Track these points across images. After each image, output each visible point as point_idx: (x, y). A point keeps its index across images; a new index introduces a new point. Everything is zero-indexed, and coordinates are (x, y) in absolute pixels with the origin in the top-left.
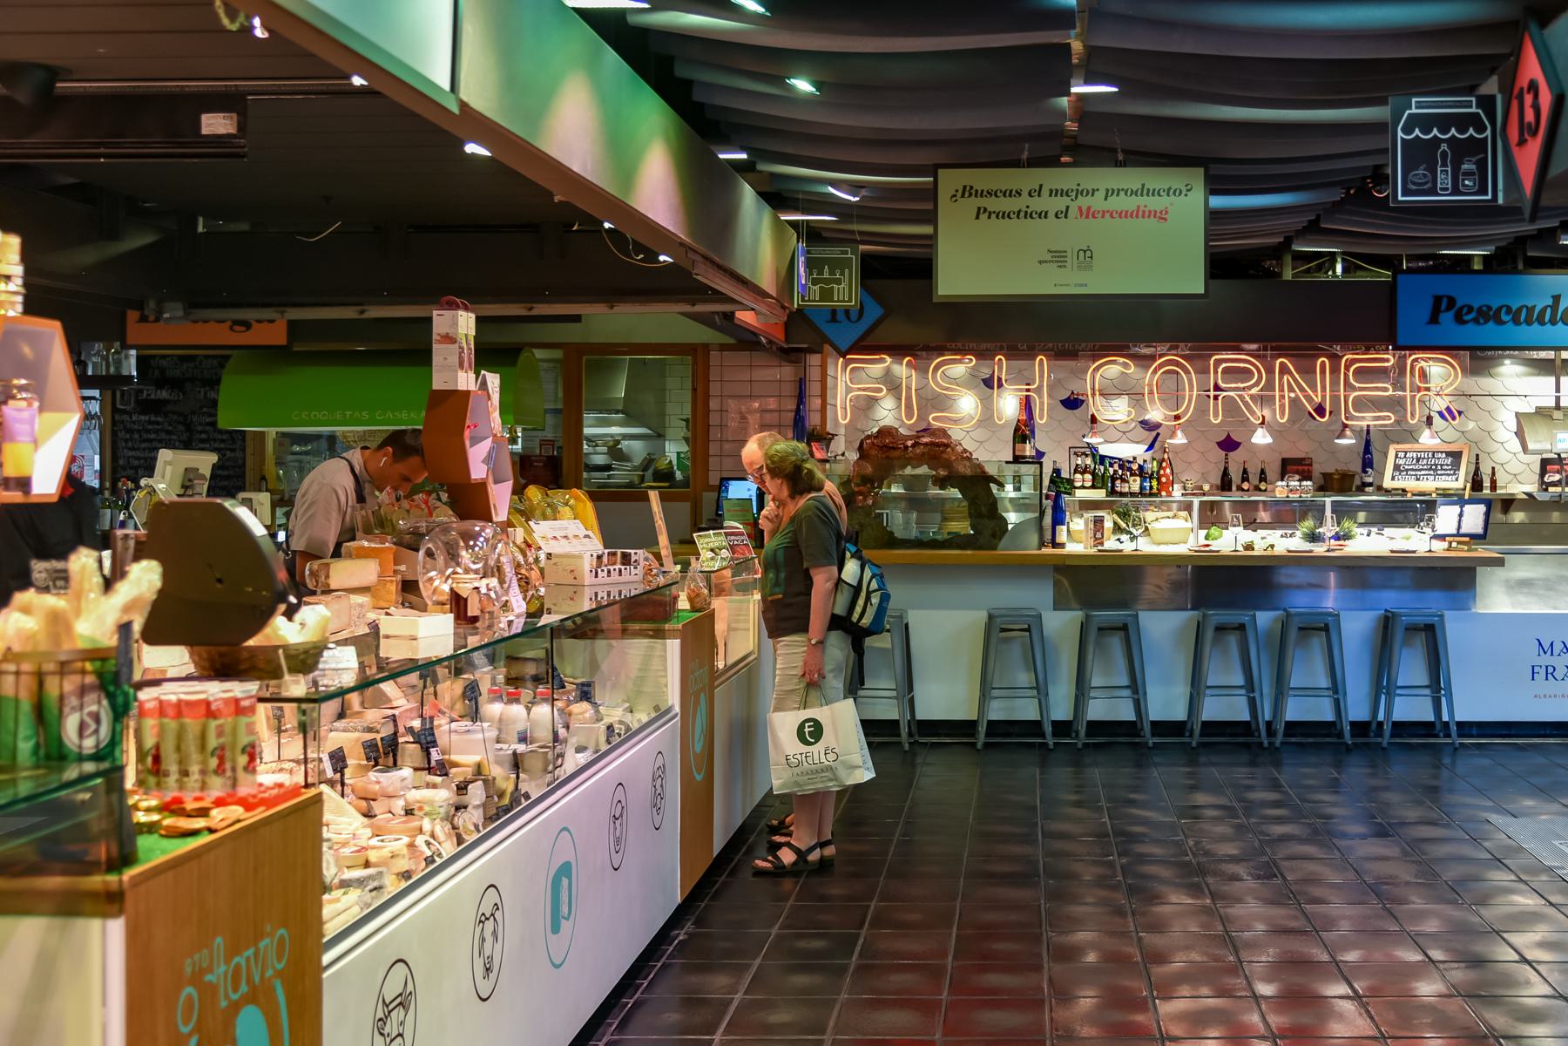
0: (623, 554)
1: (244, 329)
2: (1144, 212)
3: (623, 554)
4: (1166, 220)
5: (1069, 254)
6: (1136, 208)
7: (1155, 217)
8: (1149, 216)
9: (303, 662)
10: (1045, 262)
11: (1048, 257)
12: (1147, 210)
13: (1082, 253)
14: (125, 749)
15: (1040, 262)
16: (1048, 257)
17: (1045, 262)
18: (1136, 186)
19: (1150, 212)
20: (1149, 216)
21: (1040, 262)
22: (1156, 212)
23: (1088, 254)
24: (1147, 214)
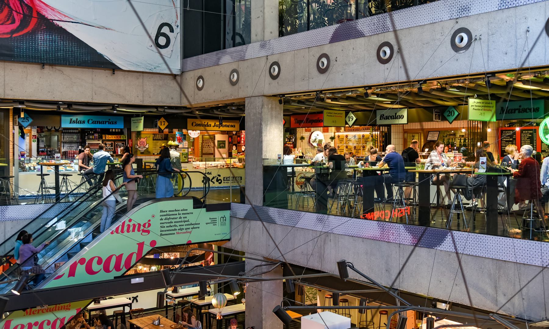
0: (481, 164)
1: (147, 233)
2: (129, 226)
3: (481, 164)
4: (148, 232)
5: (217, 219)
6: (135, 249)
7: (139, 230)
8: (134, 230)
9: (409, 155)
10: (209, 223)
11: (209, 221)
12: (131, 224)
13: (222, 218)
14: (435, 85)
15: (207, 224)
16: (209, 221)
17: (209, 223)
18: (174, 229)
19: (134, 225)
20: (134, 230)
21: (207, 224)
22: (139, 225)
23: (224, 219)
24: (131, 228)
